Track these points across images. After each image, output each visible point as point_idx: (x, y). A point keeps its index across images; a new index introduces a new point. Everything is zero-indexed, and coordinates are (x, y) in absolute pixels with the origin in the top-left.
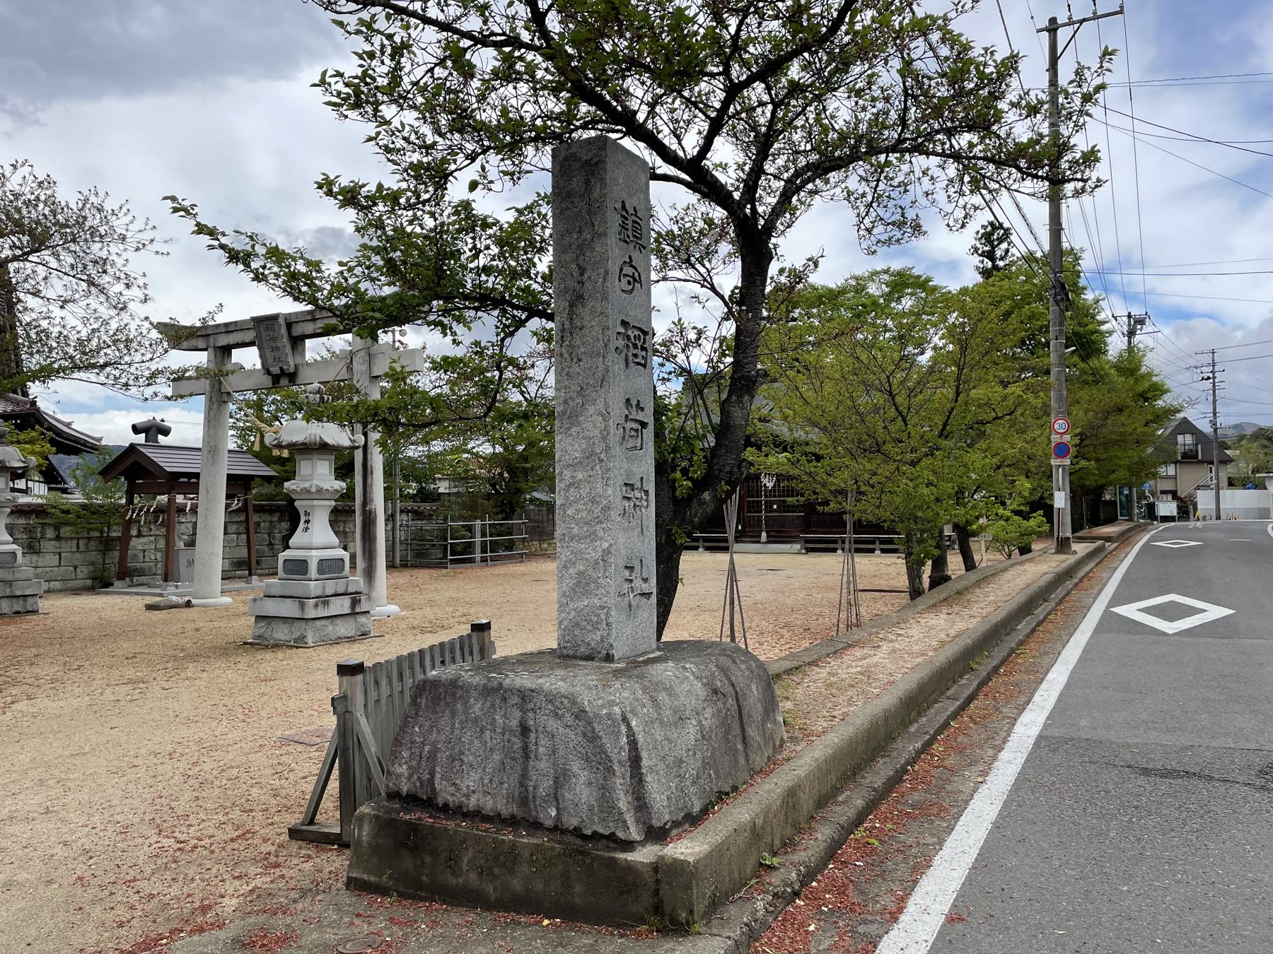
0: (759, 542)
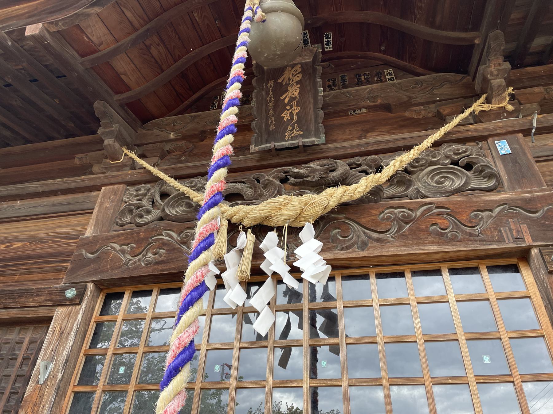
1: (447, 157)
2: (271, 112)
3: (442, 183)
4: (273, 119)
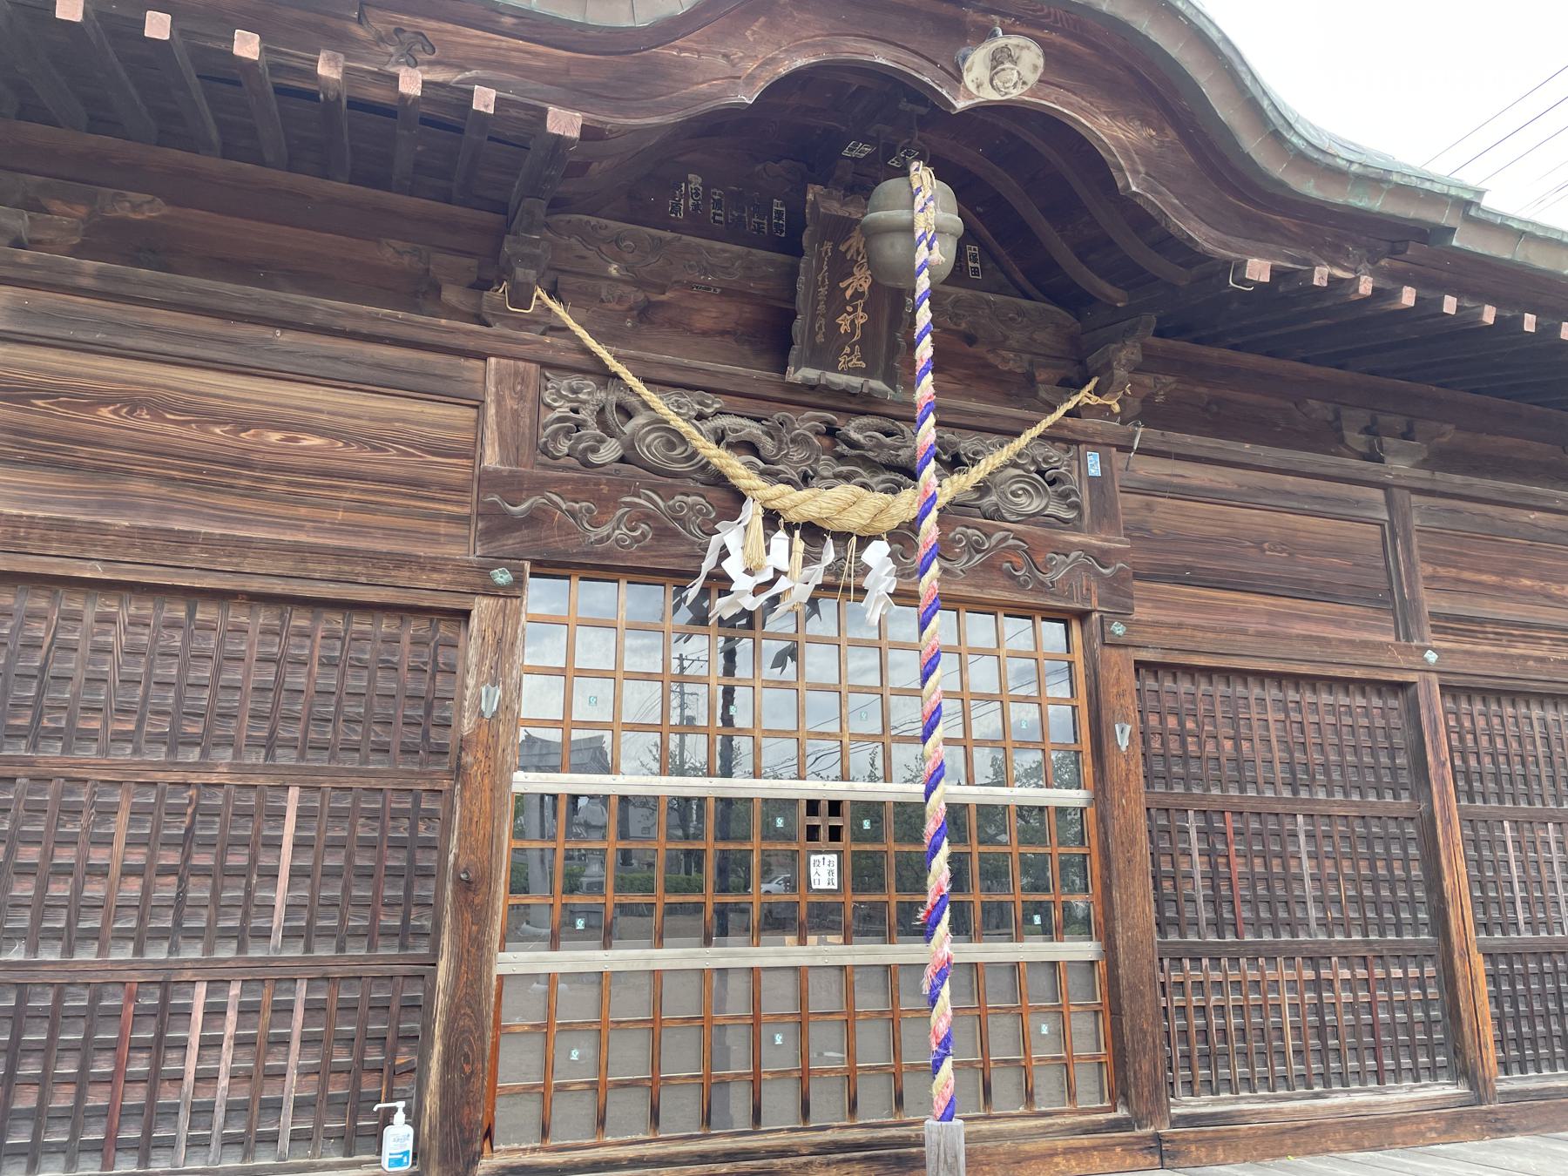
1: (1034, 461)
2: (822, 307)
3: (1019, 496)
4: (823, 321)
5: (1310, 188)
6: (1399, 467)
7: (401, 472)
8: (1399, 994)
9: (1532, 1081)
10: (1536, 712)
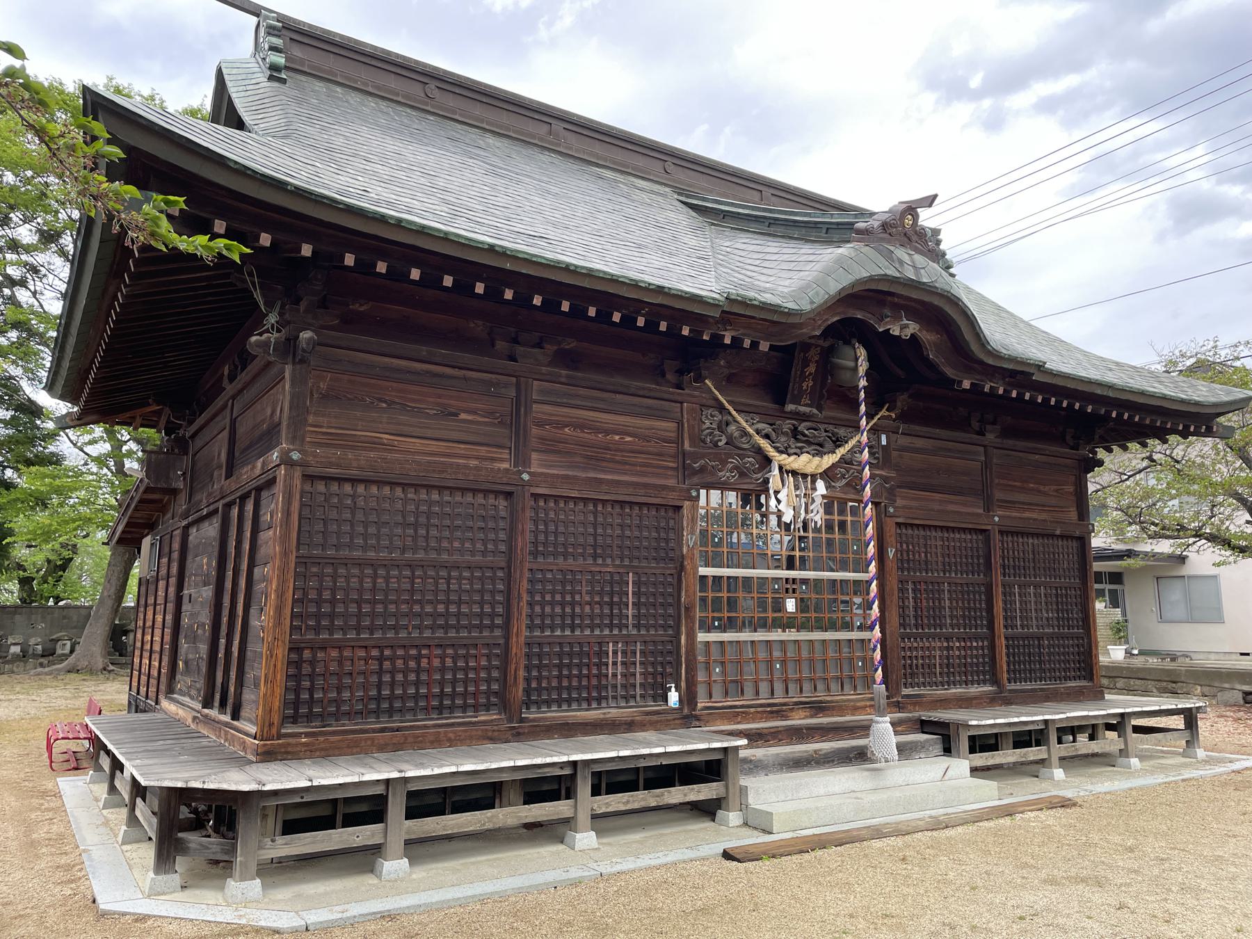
0: (860, 756)
5: (990, 361)
6: (990, 437)
7: (655, 450)
8: (975, 652)
9: (1018, 686)
10: (1031, 541)
